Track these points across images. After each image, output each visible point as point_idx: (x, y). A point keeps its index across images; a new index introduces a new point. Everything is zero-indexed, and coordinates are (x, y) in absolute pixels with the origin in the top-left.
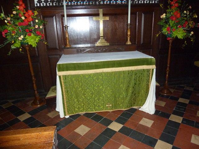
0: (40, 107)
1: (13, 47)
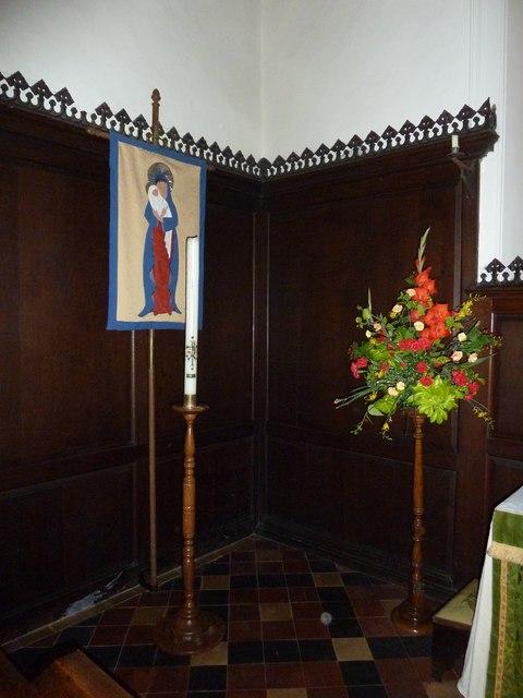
0: (419, 638)
1: (373, 411)
